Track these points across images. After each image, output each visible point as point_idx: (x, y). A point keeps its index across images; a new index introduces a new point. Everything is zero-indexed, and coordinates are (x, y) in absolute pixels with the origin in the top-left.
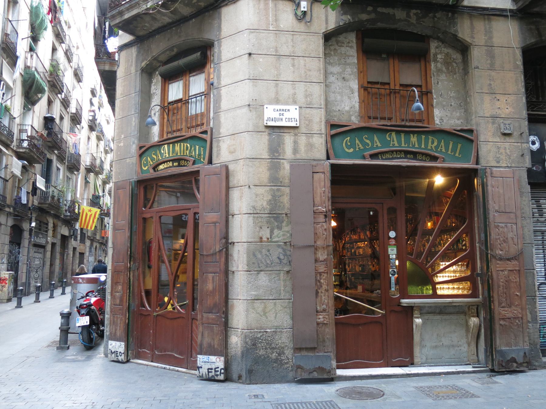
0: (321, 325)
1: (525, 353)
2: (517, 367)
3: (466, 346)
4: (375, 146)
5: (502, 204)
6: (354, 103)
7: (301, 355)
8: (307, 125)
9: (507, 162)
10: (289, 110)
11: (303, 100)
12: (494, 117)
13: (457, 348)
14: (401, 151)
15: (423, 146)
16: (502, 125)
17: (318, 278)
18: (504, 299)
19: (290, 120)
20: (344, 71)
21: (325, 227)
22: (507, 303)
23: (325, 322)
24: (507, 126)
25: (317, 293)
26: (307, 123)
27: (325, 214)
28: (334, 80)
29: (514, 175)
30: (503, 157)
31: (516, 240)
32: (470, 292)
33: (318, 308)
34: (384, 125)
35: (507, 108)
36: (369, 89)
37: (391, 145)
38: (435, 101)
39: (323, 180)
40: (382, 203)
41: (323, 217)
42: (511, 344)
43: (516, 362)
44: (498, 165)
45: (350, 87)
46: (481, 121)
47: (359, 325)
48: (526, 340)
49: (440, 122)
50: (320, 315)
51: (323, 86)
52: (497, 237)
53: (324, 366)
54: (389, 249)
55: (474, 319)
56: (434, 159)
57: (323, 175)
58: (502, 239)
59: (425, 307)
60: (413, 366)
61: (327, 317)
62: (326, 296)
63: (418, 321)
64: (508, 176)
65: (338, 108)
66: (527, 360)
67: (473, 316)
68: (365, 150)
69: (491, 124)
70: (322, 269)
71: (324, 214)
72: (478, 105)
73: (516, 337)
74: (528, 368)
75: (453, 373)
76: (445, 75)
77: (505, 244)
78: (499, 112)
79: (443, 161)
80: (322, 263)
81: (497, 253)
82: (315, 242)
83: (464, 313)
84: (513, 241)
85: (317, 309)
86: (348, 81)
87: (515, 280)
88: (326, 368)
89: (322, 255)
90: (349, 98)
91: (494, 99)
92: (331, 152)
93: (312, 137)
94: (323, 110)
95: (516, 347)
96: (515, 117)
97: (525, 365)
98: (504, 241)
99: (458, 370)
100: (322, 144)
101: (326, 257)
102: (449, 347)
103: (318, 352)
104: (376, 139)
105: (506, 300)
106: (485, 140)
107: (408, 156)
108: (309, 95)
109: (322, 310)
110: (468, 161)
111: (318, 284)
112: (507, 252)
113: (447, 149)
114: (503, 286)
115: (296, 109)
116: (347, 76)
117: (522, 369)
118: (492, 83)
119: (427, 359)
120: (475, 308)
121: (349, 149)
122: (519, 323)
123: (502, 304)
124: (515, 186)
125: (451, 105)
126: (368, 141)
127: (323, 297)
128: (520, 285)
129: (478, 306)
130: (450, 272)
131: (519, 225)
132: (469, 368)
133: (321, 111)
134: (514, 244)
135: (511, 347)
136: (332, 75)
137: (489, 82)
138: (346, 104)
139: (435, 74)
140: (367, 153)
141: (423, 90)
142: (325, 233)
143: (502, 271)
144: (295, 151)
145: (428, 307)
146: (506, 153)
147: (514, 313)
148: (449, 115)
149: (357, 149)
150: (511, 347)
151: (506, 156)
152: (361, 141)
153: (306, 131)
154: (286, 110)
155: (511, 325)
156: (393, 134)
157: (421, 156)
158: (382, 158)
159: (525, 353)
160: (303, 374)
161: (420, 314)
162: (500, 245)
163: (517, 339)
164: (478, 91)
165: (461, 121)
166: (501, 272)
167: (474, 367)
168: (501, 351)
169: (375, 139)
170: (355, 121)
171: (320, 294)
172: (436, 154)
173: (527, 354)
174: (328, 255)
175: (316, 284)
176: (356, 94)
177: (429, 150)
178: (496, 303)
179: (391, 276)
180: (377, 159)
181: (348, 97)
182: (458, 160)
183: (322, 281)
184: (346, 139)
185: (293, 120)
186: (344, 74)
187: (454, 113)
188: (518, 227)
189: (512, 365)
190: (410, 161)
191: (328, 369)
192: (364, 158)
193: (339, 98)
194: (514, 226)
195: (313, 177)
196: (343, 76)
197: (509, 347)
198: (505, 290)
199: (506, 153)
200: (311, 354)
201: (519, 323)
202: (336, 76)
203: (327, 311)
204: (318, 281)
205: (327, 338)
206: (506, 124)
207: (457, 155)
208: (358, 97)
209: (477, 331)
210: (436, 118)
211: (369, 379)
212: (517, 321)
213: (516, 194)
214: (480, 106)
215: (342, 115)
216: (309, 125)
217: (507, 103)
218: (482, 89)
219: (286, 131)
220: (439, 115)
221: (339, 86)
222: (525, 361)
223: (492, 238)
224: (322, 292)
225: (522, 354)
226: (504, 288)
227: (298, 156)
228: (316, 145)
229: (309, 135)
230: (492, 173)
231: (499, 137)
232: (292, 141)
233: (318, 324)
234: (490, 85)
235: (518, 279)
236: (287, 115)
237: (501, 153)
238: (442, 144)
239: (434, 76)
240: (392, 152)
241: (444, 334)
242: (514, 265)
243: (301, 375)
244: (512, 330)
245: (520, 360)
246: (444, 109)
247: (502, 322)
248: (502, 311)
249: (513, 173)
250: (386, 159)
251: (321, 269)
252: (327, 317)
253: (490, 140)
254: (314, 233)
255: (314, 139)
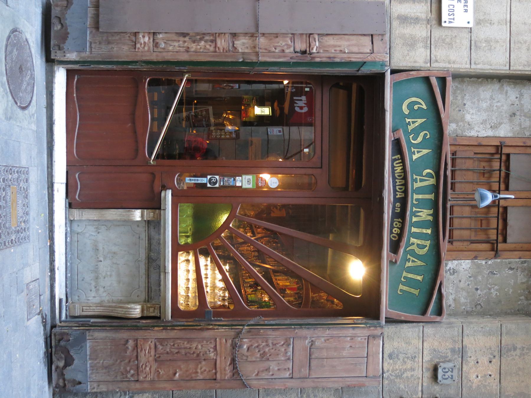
0: (134, 39)
1: (80, 383)
2: (57, 367)
3: (97, 300)
4: (413, 150)
5: (324, 354)
6: (476, 128)
7: (87, 28)
8: (444, 40)
9: (390, 372)
10: (466, 11)
11: (482, 36)
12: (463, 352)
13: (93, 284)
14: (406, 192)
15: (414, 230)
16: (451, 365)
17: (207, 38)
18: (168, 350)
19: (452, 12)
20: (525, 116)
21: (287, 51)
22: (161, 354)
23: (138, 46)
24: (449, 373)
25: (184, 35)
26: (447, 40)
27: (308, 52)
28: (511, 98)
29: (371, 377)
30: (398, 365)
31: (264, 375)
32: (182, 308)
33: (161, 36)
34: (446, 164)
35: (477, 377)
36: (498, 156)
37: (415, 177)
38: (483, 262)
39: (361, 51)
40: (321, 168)
41: (303, 49)
42: (96, 359)
43: (65, 366)
44: (386, 356)
45: (500, 124)
46: (456, 331)
47: (134, 123)
48: (101, 386)
49: (450, 269)
50: (149, 38)
51: (505, 68)
52: (270, 342)
53: (69, 41)
54: (250, 177)
55: (138, 310)
56: (395, 247)
57: (368, 51)
58: (267, 350)
59: (159, 234)
60: (67, 206)
61: (146, 48)
62: (178, 49)
63: (137, 215)
64: (370, 368)
65: (468, 104)
66: (69, 386)
67: (142, 310)
68: (407, 133)
69: (451, 346)
70: (222, 43)
71: (308, 50)
72: (482, 326)
73: (106, 368)
74: (56, 387)
75: (52, 261)
76: (523, 281)
77: (258, 355)
78: (472, 363)
79: (391, 262)
80: (231, 45)
81: (245, 340)
82: (263, 34)
83: (149, 299)
84: (263, 371)
85: (159, 33)
86: (511, 121)
87: (199, 371)
88: (67, 44)
89: (244, 44)
90: (484, 122)
91: (492, 354)
92: (402, 77)
93: (426, 47)
94: (468, 66)
95: (91, 367)
96: (464, 389)
97: (61, 383)
98: (264, 354)
99: (57, 271)
100: (415, 62)
101: (240, 51)
102: (96, 270)
103: (91, 32)
104: (425, 151)
105: (167, 353)
106: (425, 335)
107: (398, 204)
108: (491, 46)
109: (157, 41)
110: (391, 305)
111: (198, 37)
112: (245, 358)
113: (410, 270)
114: (190, 348)
115: (468, 23)
116: (517, 120)
117: (54, 376)
118: (518, 352)
119: (78, 234)
120: (156, 314)
121: (408, 106)
122: (129, 376)
123: (161, 345)
124: (353, 379)
125: (477, 289)
126: (420, 139)
127: (176, 44)
128: (191, 380)
129: (159, 318)
130: (214, 278)
131: (291, 384)
132: (60, 292)
133: (466, 64)
134: (258, 372)
135: (90, 359)
136: (518, 96)
137: (519, 346)
138: (474, 117)
139: (525, 265)
140: (401, 135)
141: (499, 245)
142: (277, 51)
143: (215, 348)
144: (404, 19)
145: (159, 240)
146: (406, 370)
147: (146, 366)
148: (462, 285)
149: (408, 120)
150: (90, 359)
151: (400, 370)
152: (422, 127)
153: (435, 37)
154: (467, 6)
155: (127, 361)
156: (432, 181)
157: (398, 226)
158: (395, 160)
159: (80, 383)
160: (58, 9)
161: (148, 221)
162: (257, 347)
163: (104, 371)
164: (504, 328)
165: (453, 305)
166: (212, 346)
167: (61, 300)
168: (84, 340)
169: (424, 150)
170: (450, 129)
171: (182, 39)
172: (402, 251)
173: (78, 387)
174: (243, 53)
175: (198, 34)
176: (490, 133)
177: (409, 240)
178: (163, 335)
179: (209, 177)
180: (392, 152)
181: (486, 120)
182: (393, 287)
183: (202, 43)
184: (423, 103)
185: (452, 17)
186: (521, 116)
187: (464, 294)
188: (286, 380)
189: (61, 358)
190: (391, 206)
191: (65, 47)
192: (394, 130)
193: (484, 105)
194: (288, 373)
195: (364, 35)
196: (518, 113)
197: (90, 355)
198: (183, 352)
199: (406, 370)
200: (89, 22)
201: (129, 376)
202: (517, 102)
203: (155, 50)
204: (202, 36)
205: (112, 48)
206: (452, 372)
207: (401, 287)
208: (485, 135)
209: (119, 315)
210: (455, 262)
211: (47, 121)
212: (132, 372)
213: (340, 379)
214: (480, 329)
215: (457, 109)
216: (444, 43)
217: (485, 376)
218: (507, 334)
219: (434, 6)
220: (461, 269)
221: (502, 106)
222: (66, 382)
223: (270, 332)
224: (185, 42)
225: (79, 377)
226: (187, 350)
227: (395, 23)
228: (414, 53)
229: (429, 43)
230: (374, 337)
231: (431, 360)
232: (419, 15)
233: (136, 34)
234: (515, 349)
235: (201, 377)
236: (459, 7)
237: (405, 362)
238: (419, 263)
239: (522, 263)
240: (405, 178)
241: (116, 263)
242: (225, 370)
243: (57, 6)
244: (119, 361)
245: (69, 373)
246: (470, 277)
247: (131, 343)
248: (150, 345)
249: (375, 377)
250: (393, 167)
251: (221, 43)
252: (146, 48)
253: (425, 344)
254: (276, 34)
255: (423, 50)
